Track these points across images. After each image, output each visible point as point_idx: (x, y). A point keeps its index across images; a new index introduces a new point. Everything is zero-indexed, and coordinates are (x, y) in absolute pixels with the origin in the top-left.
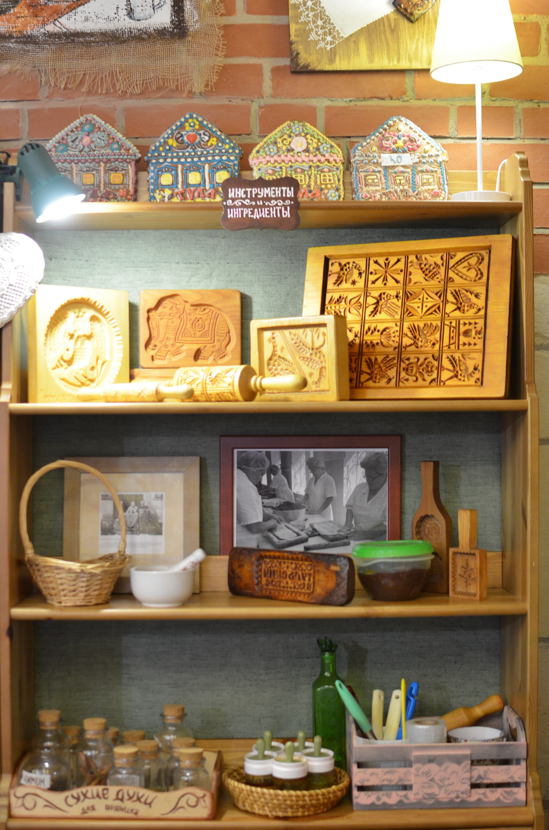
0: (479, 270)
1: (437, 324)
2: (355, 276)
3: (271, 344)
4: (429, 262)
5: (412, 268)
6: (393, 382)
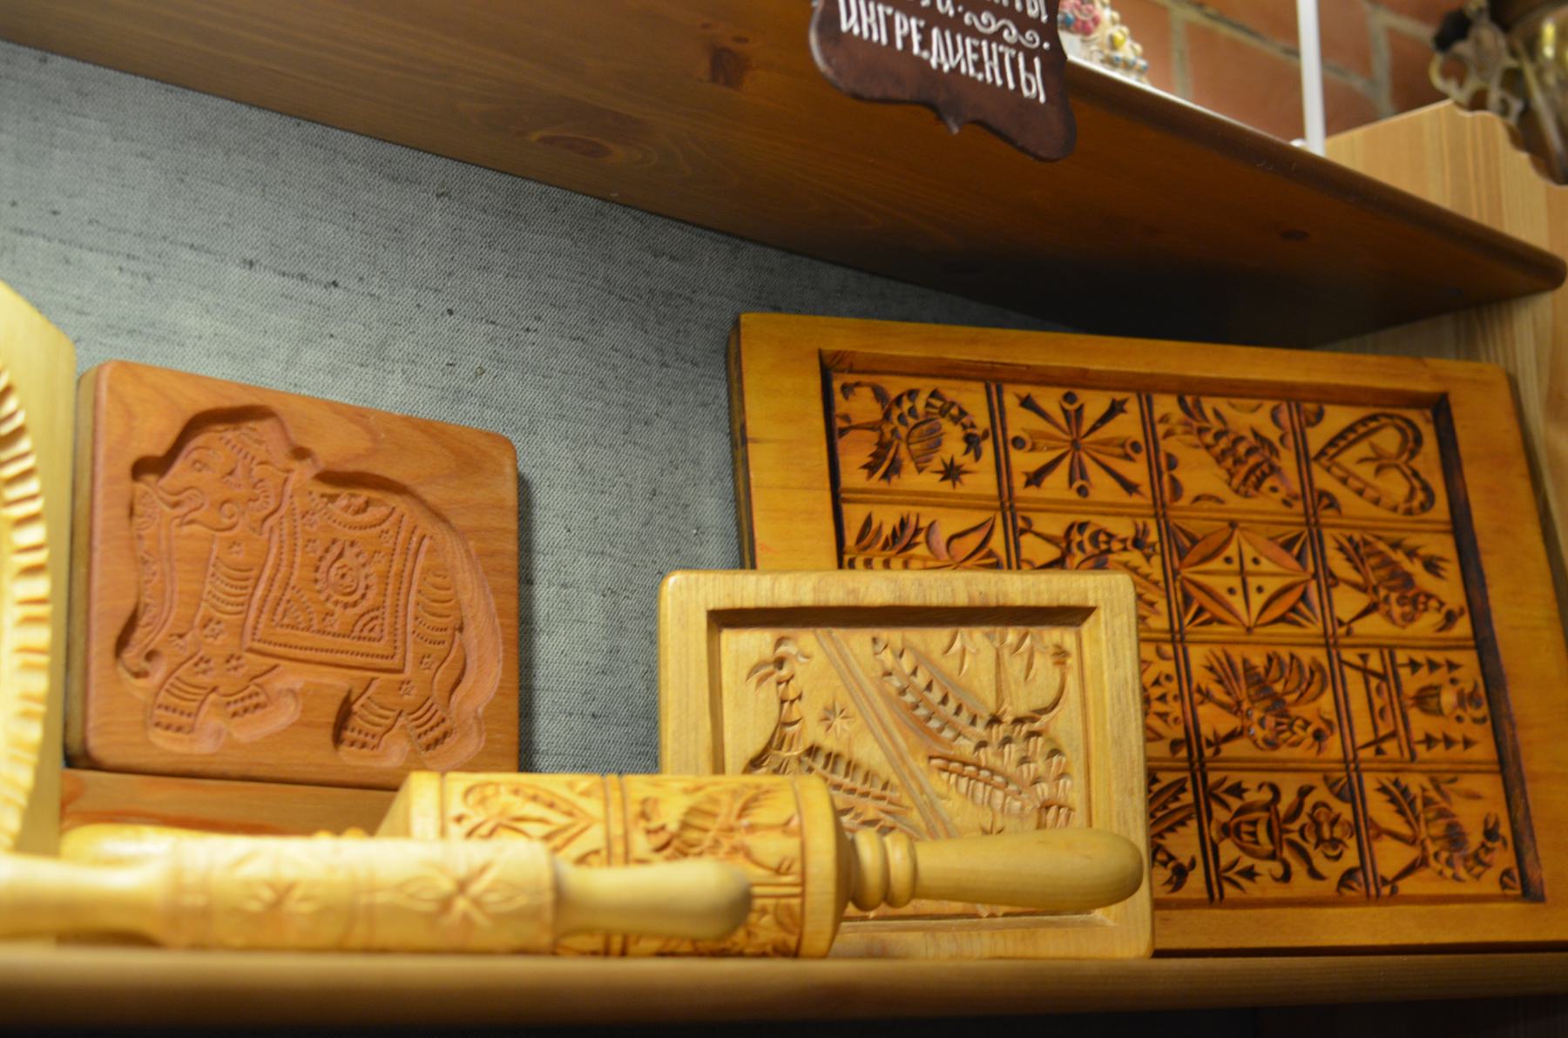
0: (1416, 474)
1: (1314, 660)
2: (953, 446)
3: (770, 692)
4: (1231, 426)
5: (1172, 440)
6: (1196, 880)
